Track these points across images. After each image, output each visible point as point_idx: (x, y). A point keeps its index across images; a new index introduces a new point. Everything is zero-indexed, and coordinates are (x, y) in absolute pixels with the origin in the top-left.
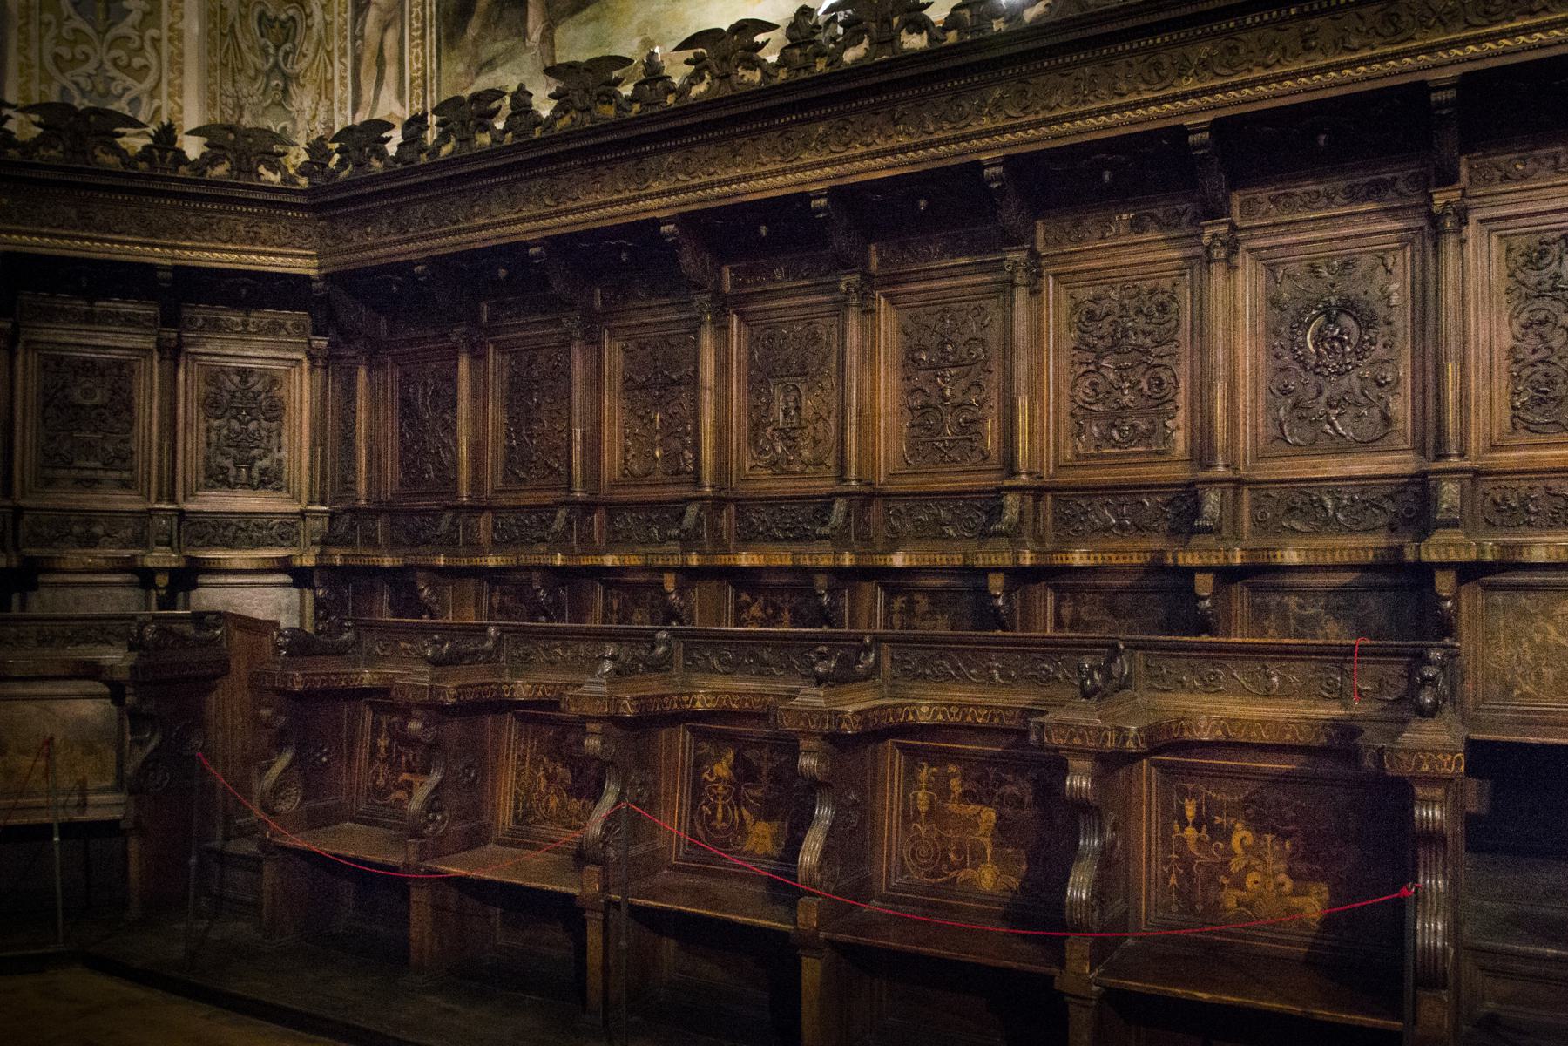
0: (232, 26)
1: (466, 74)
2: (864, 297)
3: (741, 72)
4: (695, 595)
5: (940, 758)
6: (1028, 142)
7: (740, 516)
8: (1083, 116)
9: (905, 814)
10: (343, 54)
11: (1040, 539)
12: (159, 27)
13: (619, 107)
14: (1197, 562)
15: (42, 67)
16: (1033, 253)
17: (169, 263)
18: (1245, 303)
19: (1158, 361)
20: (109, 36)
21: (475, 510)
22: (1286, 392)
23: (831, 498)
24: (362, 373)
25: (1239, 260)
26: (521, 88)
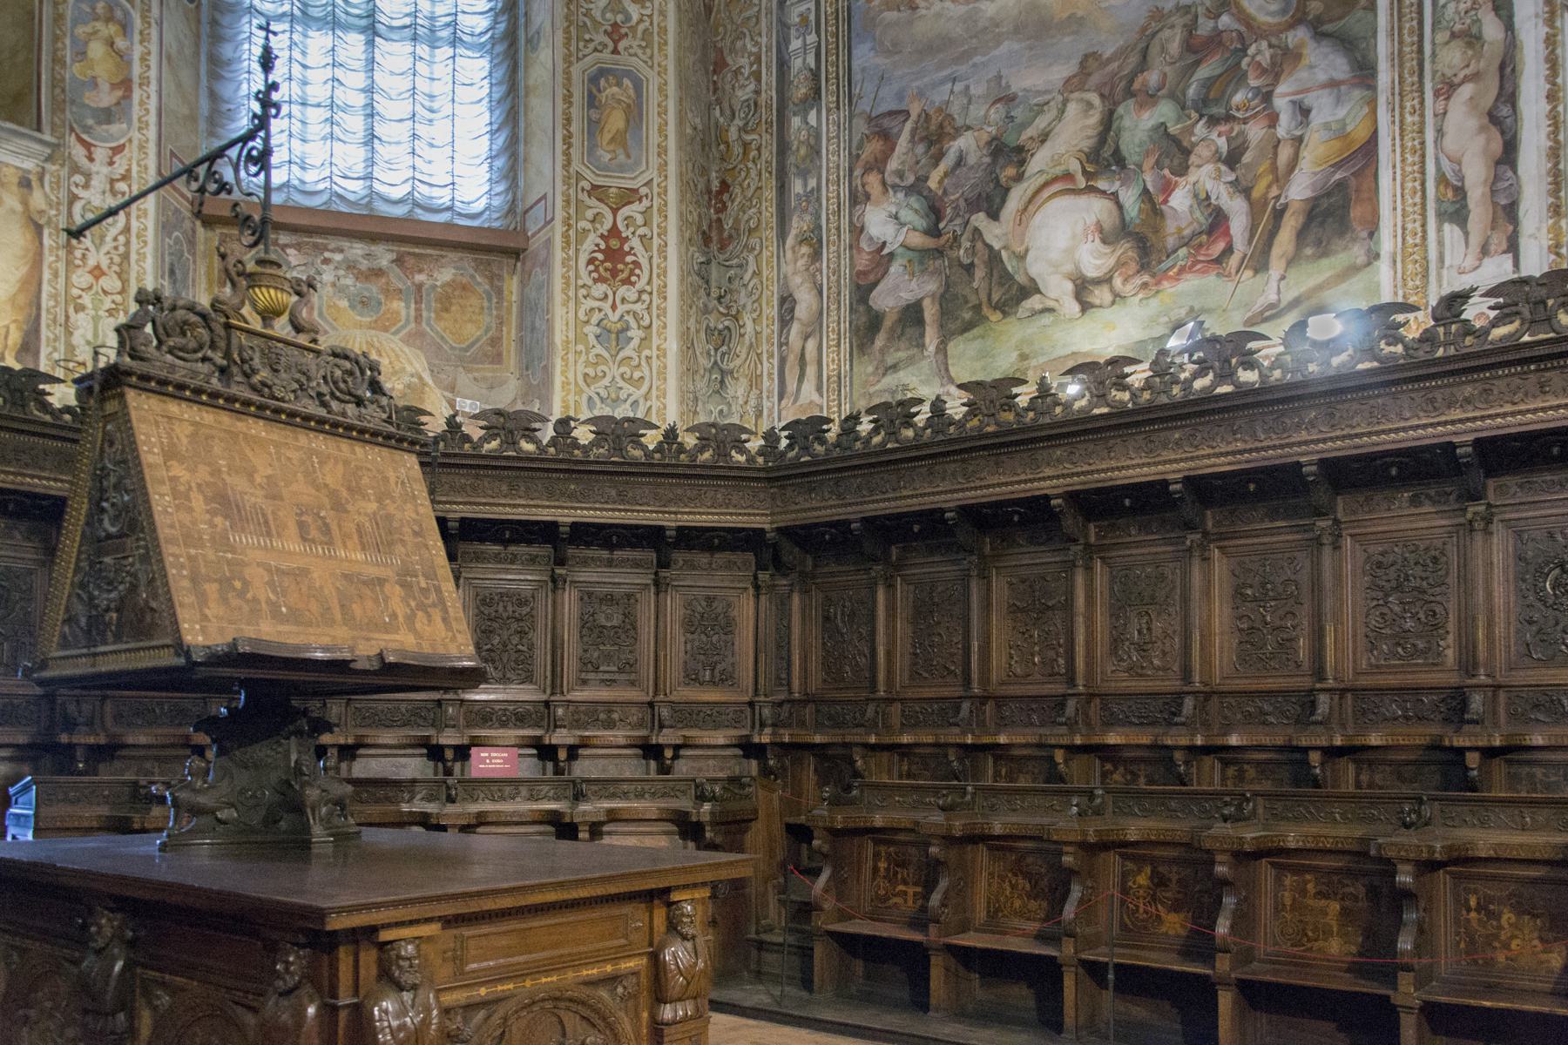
1: (874, 374)
2: (1203, 548)
3: (1114, 392)
4: (1074, 764)
5: (1299, 870)
6: (1336, 449)
7: (1104, 708)
8: (1378, 433)
9: (1276, 908)
10: (771, 356)
11: (1343, 726)
12: (650, 349)
13: (1017, 414)
14: (1468, 744)
15: (576, 383)
16: (1337, 522)
17: (673, 524)
18: (1498, 558)
19: (1432, 598)
20: (619, 358)
21: (889, 701)
22: (1531, 622)
23: (1179, 697)
24: (796, 600)
25: (1493, 527)
26: (938, 397)
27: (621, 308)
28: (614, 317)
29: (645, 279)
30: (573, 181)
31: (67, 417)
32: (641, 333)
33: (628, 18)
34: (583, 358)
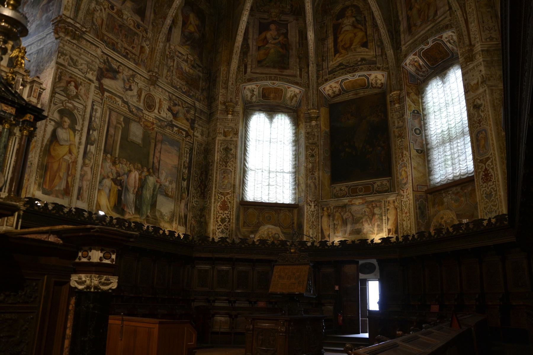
15: (483, 210)
27: (490, 188)
28: (488, 191)
29: (494, 178)
30: (476, 161)
31: (395, 244)
32: (495, 193)
33: (481, 116)
34: (483, 203)
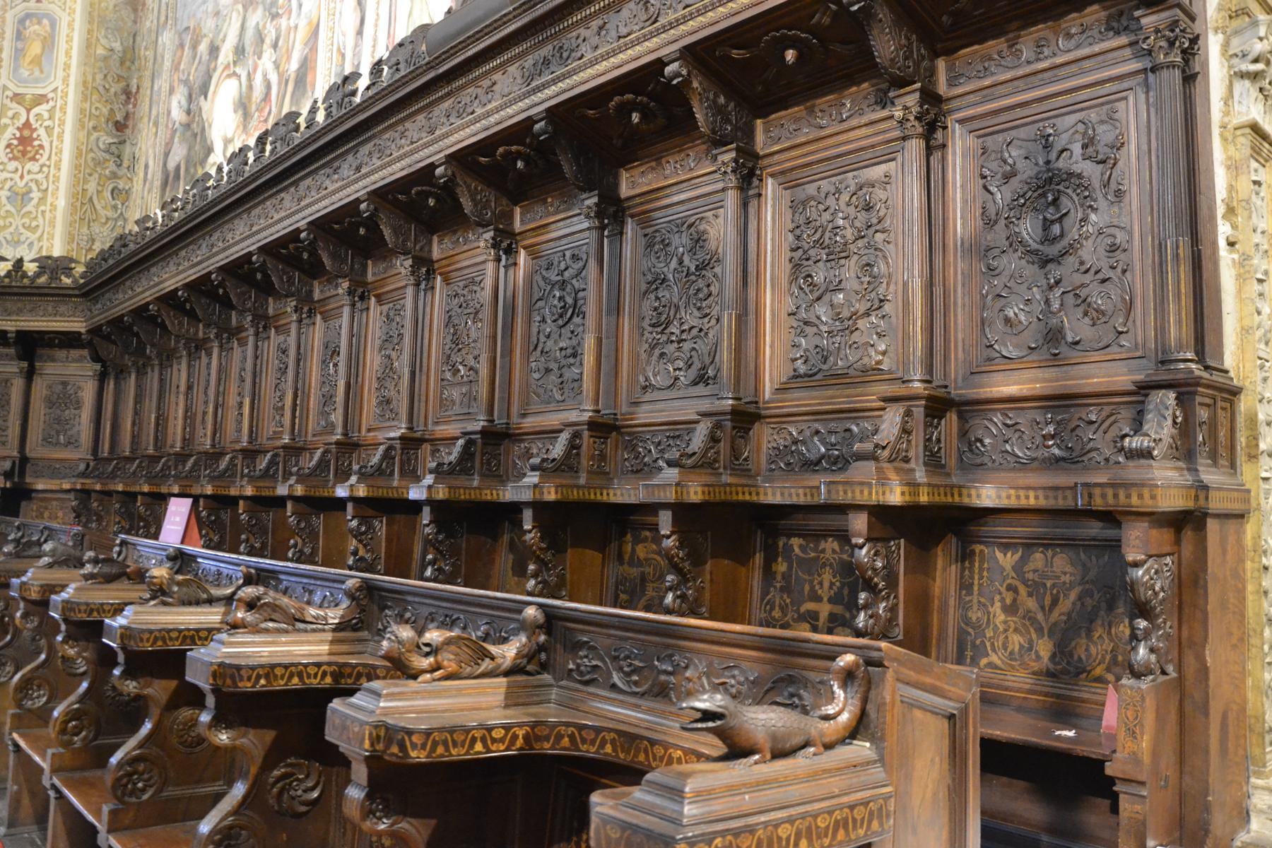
0: (91, 199)
20: (23, 212)
